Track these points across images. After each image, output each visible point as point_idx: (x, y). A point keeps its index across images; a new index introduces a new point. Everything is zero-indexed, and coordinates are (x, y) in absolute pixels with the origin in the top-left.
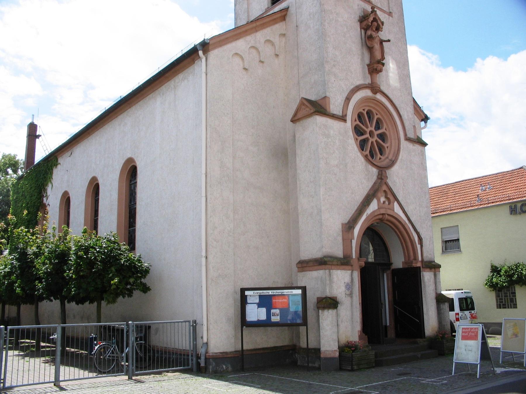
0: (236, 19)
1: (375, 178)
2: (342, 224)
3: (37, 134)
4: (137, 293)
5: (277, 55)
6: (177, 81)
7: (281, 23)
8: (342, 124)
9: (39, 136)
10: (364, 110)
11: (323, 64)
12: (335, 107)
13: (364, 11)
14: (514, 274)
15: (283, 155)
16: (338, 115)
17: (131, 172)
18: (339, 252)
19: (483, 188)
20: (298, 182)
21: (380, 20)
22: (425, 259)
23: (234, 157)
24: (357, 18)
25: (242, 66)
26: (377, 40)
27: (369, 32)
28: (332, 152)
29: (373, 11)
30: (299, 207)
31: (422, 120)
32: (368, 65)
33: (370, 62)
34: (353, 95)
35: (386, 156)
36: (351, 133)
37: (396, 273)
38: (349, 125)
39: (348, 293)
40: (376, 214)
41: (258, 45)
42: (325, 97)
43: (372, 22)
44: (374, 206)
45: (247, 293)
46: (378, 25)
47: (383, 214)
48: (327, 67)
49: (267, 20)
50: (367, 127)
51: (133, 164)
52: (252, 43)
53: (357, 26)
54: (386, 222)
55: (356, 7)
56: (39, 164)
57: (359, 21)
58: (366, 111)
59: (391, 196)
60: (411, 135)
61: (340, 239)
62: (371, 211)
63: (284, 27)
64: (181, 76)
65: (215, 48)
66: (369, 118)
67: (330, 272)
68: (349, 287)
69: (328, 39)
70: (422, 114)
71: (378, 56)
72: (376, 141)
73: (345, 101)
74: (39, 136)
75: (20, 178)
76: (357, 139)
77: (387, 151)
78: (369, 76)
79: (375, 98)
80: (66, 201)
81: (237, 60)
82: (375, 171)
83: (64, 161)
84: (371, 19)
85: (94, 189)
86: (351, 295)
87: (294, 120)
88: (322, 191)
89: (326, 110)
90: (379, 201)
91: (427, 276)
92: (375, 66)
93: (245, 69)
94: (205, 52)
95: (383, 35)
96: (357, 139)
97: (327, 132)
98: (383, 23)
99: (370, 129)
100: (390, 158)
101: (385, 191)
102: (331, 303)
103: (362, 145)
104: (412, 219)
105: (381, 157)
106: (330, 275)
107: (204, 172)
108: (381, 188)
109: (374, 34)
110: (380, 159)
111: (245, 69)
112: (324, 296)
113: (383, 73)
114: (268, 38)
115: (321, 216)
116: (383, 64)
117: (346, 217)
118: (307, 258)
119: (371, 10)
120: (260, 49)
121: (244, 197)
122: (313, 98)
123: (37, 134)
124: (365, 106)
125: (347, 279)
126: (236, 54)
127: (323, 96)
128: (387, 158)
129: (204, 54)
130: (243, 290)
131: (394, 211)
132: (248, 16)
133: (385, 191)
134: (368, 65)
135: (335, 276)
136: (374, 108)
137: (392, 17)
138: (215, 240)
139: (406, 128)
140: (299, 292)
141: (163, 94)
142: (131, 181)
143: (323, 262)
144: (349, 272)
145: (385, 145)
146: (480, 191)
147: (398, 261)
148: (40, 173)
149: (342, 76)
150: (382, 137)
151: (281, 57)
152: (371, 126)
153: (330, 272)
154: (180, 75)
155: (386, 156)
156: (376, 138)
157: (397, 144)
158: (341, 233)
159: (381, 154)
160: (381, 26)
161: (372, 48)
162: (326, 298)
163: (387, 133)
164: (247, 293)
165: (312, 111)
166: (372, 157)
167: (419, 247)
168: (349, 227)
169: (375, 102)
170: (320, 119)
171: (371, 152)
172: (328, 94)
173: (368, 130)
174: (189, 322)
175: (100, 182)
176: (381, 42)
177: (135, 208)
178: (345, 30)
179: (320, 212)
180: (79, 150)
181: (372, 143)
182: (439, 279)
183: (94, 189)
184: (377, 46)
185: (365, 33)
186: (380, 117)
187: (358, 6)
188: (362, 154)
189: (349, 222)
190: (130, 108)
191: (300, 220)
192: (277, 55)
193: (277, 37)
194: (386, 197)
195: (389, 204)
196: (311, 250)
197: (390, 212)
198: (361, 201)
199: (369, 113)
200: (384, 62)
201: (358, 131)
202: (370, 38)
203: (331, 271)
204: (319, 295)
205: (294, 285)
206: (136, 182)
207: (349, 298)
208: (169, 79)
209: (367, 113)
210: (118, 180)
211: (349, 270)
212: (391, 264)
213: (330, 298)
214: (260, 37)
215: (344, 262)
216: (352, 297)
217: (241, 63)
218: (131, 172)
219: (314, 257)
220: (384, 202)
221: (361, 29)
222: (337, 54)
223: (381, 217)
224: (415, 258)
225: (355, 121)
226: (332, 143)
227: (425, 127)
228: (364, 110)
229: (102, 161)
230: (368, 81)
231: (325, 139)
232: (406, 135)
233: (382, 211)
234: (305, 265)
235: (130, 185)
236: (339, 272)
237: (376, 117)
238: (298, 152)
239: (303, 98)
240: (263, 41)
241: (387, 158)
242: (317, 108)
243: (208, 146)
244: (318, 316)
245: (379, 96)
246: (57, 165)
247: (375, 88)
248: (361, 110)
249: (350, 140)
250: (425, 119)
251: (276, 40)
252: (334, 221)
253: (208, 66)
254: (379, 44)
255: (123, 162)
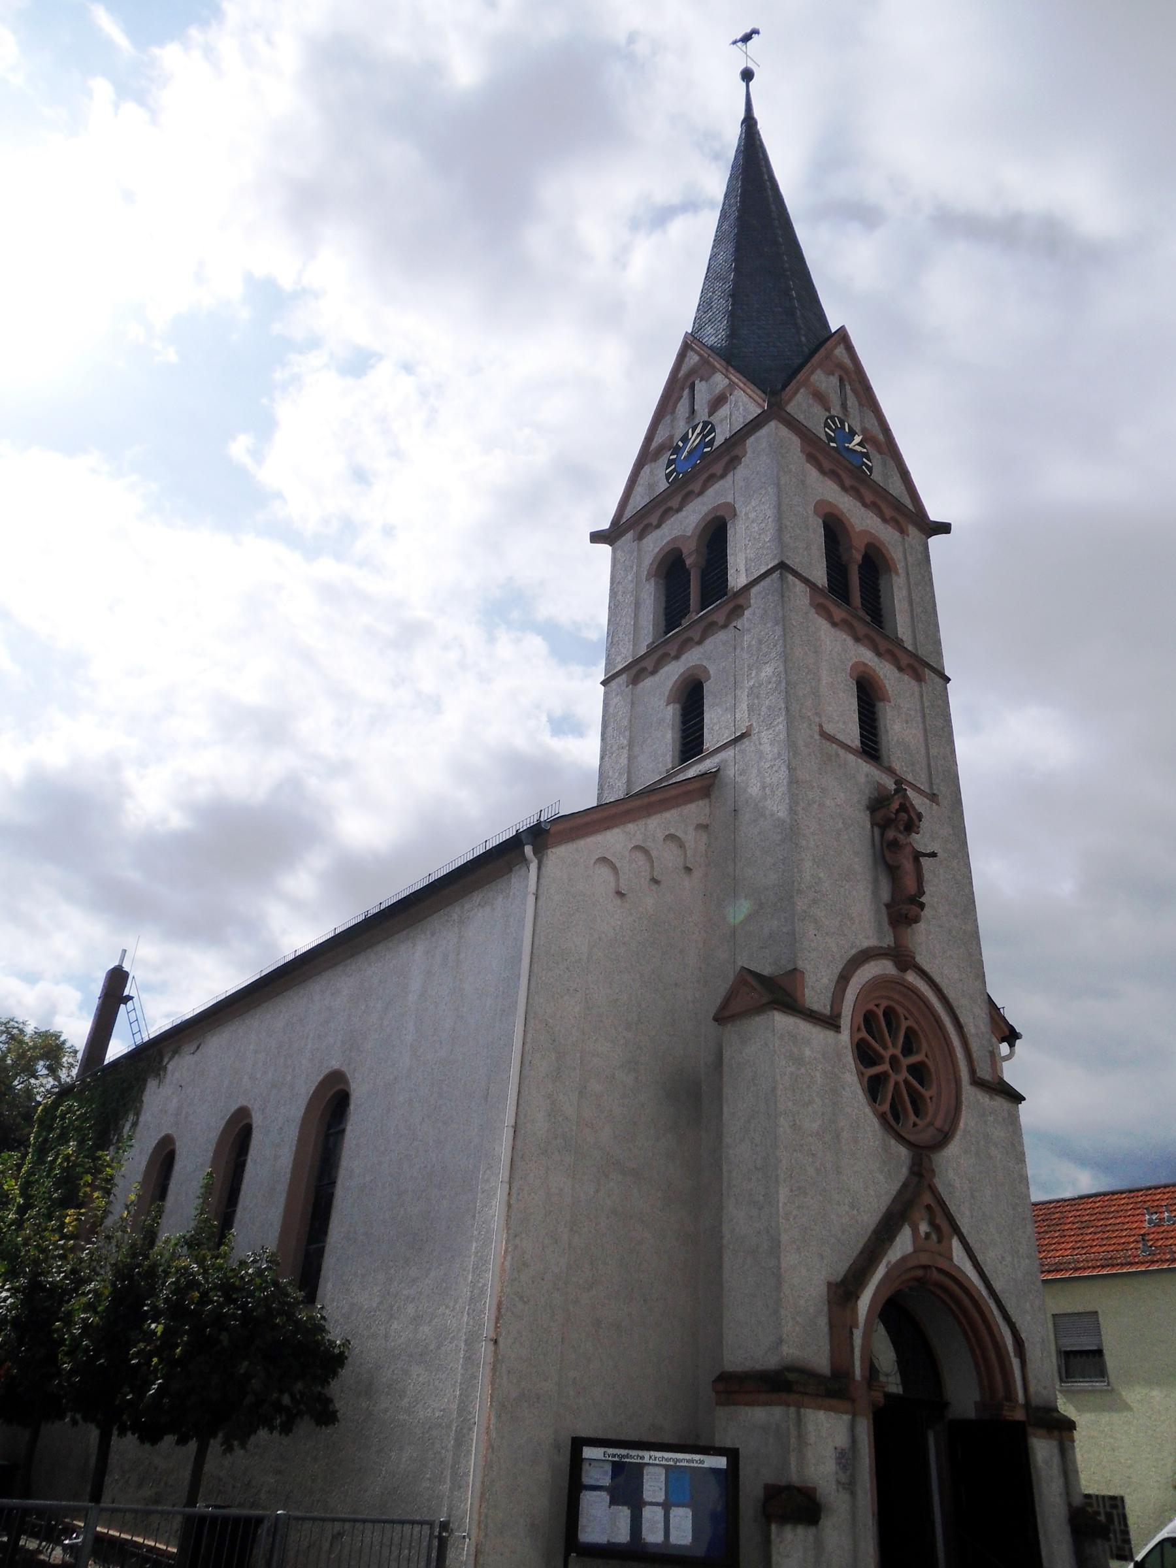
0: (601, 787)
1: (904, 1171)
2: (830, 1284)
3: (126, 993)
4: (305, 1426)
5: (688, 870)
6: (467, 906)
7: (701, 803)
8: (830, 1034)
9: (129, 998)
10: (877, 1006)
11: (792, 897)
12: (816, 994)
13: (879, 787)
14: (113, 1168)
15: (693, 1099)
16: (821, 1014)
17: (332, 1105)
18: (819, 1358)
19: (1154, 1217)
20: (725, 1168)
21: (914, 808)
22: (1035, 1401)
23: (580, 1092)
24: (865, 802)
25: (613, 885)
26: (908, 849)
27: (891, 834)
28: (806, 1099)
29: (900, 790)
30: (726, 1230)
31: (1003, 1040)
32: (887, 906)
33: (893, 898)
34: (855, 970)
35: (928, 1119)
36: (849, 1059)
37: (960, 1431)
38: (845, 1037)
39: (844, 1478)
40: (911, 1264)
41: (649, 845)
42: (795, 969)
43: (897, 811)
44: (903, 1245)
45: (589, 1452)
46: (911, 819)
47: (925, 1267)
48: (801, 904)
49: (673, 792)
50: (885, 1048)
51: (341, 1086)
52: (638, 840)
53: (864, 819)
54: (932, 1288)
55: (862, 779)
56: (116, 1063)
57: (868, 808)
58: (882, 1008)
59: (945, 1223)
60: (984, 1073)
61: (823, 1322)
62: (899, 1255)
63: (707, 810)
64: (477, 897)
65: (559, 843)
66: (889, 1024)
67: (798, 1414)
68: (847, 1459)
69: (804, 842)
70: (1002, 1025)
71: (910, 884)
72: (906, 1081)
73: (838, 982)
74: (129, 998)
75: (65, 1092)
76: (862, 1074)
77: (931, 1108)
78: (891, 931)
79: (904, 980)
80: (165, 1158)
81: (604, 872)
82: (903, 1152)
83: (180, 1067)
84: (895, 805)
85: (238, 1136)
86: (850, 1486)
87: (723, 1016)
88: (783, 1193)
89: (795, 1001)
90: (915, 1231)
91: (1042, 1449)
92: (903, 909)
93: (620, 894)
94: (539, 851)
95: (922, 841)
96: (862, 1074)
97: (795, 1050)
98: (920, 816)
99: (892, 1051)
100: (938, 1123)
101: (928, 1207)
102: (798, 1506)
103: (874, 1088)
104: (997, 1286)
105: (918, 1121)
106: (799, 1422)
107: (509, 1119)
108: (917, 1197)
109: (901, 837)
110: (915, 1125)
111: (620, 894)
112: (783, 1483)
113: (921, 926)
114: (672, 831)
115: (778, 1258)
116: (922, 906)
117: (839, 1267)
118: (739, 1369)
119: (893, 787)
120: (654, 854)
121: (597, 1191)
122: (766, 971)
123: (126, 993)
124: (882, 997)
125: (841, 1439)
126: (603, 860)
127: (790, 967)
128: (931, 1124)
129: (535, 853)
130: (578, 1444)
131: (951, 1259)
132: (629, 782)
133: (928, 1207)
134: (887, 906)
135: (811, 1427)
136: (901, 1004)
137: (938, 804)
138: (521, 1298)
139: (975, 1055)
140: (721, 1462)
141: (433, 934)
142: (329, 1127)
143: (781, 1384)
144: (846, 1418)
145: (927, 1094)
146: (1146, 1225)
147: (963, 1397)
148: (114, 1087)
149: (836, 924)
150: (919, 1072)
151: (698, 874)
152: (894, 1045)
153: (798, 1414)
154: (475, 894)
155: (928, 1119)
156: (905, 1074)
157: (954, 1092)
158: (826, 1308)
159: (917, 1114)
160: (916, 821)
161: (898, 867)
162: (789, 1488)
163: (930, 1063)
164: (589, 1452)
165: (764, 1000)
166: (897, 1118)
167: (1016, 1363)
168: (844, 1292)
169: (903, 989)
170: (782, 1020)
171: (893, 1106)
172: (800, 965)
173: (887, 1055)
174: (431, 1524)
175: (257, 1120)
176: (917, 856)
177: (332, 1195)
178: (840, 825)
179: (775, 1247)
180: (216, 1043)
181: (897, 1084)
182: (1074, 1462)
183: (238, 1136)
184: (908, 865)
185: (882, 835)
186: (916, 1027)
187: (867, 776)
188: (875, 1112)
189: (844, 1282)
190: (352, 956)
191: (727, 1264)
192: (688, 870)
193: (691, 830)
194: (932, 1224)
195: (940, 1241)
196: (749, 1346)
197: (945, 1265)
198: (872, 1227)
199: (889, 1013)
200: (923, 899)
201: (865, 1055)
202: (894, 845)
203: (802, 1410)
204: (769, 1476)
205: (702, 1443)
206: (343, 1131)
207: (846, 1497)
208: (450, 902)
209: (885, 1014)
210: (298, 1121)
211: (846, 1413)
212: (945, 1405)
213: (799, 1490)
214: (655, 826)
215: (832, 1388)
216: (853, 1494)
217: (612, 879)
218: (332, 1105)
219: (758, 1367)
220: (928, 1236)
221: (872, 825)
222: (822, 875)
223: (920, 1273)
224: (1010, 1395)
225: (859, 1029)
226: (803, 1077)
227: (1008, 1057)
228: (877, 1006)
229: (270, 1078)
230: (888, 941)
231: (793, 1069)
232: (972, 1071)
233: (924, 1259)
234: (739, 1387)
235: (327, 1136)
236: (821, 1415)
237: (904, 1025)
238: (727, 1091)
239: (743, 968)
240: (660, 836)
241: (931, 1124)
242: (777, 992)
243: (526, 1062)
244: (767, 1541)
245: (911, 977)
246: (159, 1069)
247: (903, 959)
248: (871, 1006)
249: (848, 1075)
250: (1011, 1036)
251: (690, 836)
252: (807, 1276)
253: (542, 881)
254: (911, 859)
255: (320, 1078)
